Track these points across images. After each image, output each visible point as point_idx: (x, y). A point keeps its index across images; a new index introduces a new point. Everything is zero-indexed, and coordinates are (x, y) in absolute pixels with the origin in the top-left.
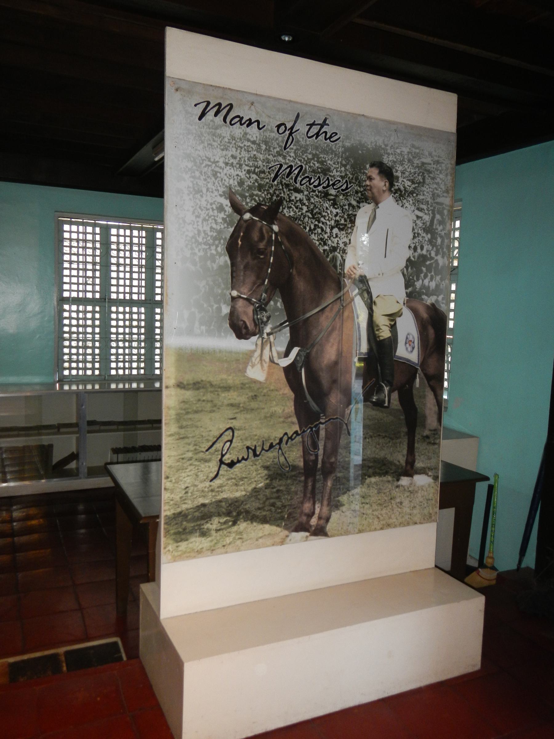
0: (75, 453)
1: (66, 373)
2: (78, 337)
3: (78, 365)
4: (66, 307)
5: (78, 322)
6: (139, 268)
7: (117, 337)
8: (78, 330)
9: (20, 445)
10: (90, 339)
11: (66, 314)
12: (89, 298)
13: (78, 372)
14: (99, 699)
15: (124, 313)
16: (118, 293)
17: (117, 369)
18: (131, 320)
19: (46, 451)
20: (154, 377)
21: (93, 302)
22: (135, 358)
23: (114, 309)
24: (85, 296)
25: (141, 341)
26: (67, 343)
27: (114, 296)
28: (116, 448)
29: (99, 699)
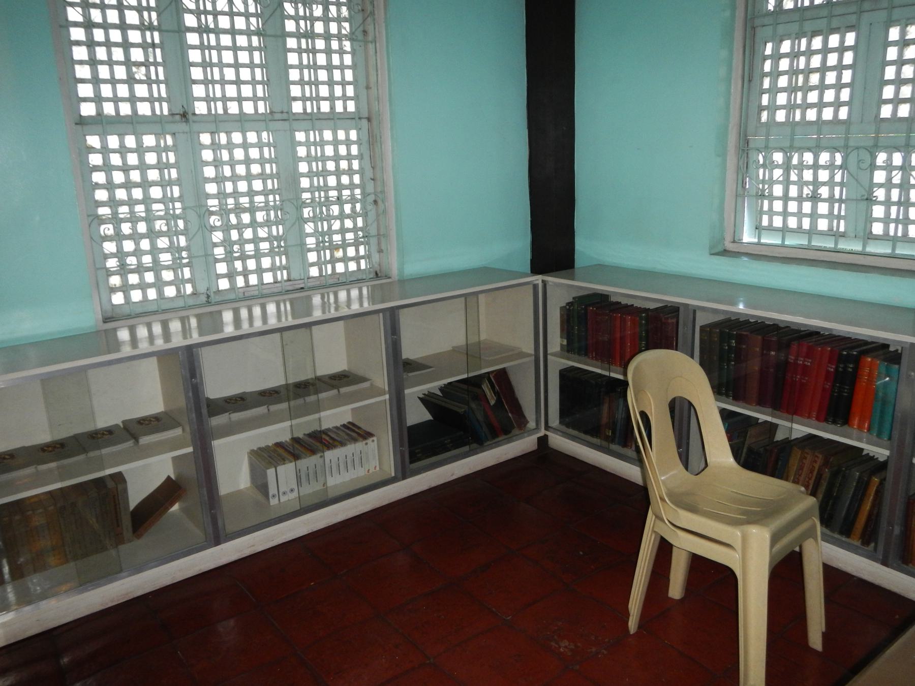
0: (173, 477)
1: (118, 299)
2: (132, 212)
3: (142, 278)
4: (93, 141)
5: (127, 176)
6: (314, 48)
7: (252, 202)
8: (129, 195)
9: (286, 438)
10: (162, 213)
11: (95, 159)
12: (144, 116)
13: (145, 295)
14: (897, 617)
15: (123, 151)
16: (98, 99)
17: (126, 288)
18: (143, 167)
19: (109, 490)
20: (311, 284)
21: (155, 123)
22: (166, 258)
23: (205, 138)
24: (319, 108)
25: (176, 217)
26: (108, 229)
27: (88, 110)
28: (260, 449)
29: (897, 617)
